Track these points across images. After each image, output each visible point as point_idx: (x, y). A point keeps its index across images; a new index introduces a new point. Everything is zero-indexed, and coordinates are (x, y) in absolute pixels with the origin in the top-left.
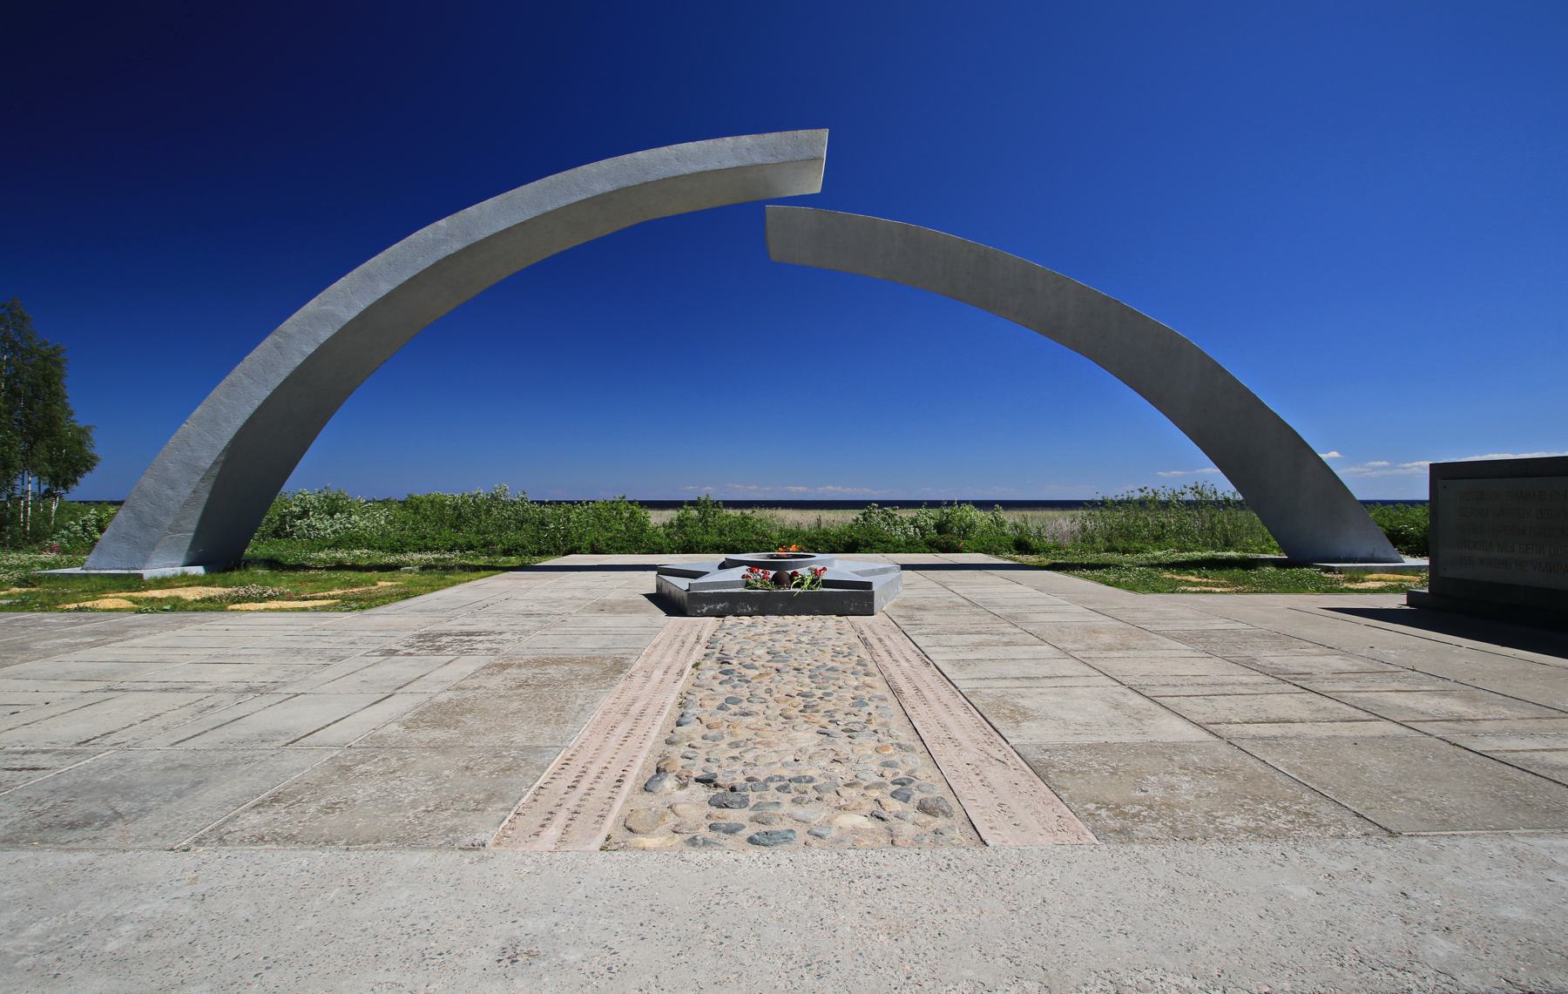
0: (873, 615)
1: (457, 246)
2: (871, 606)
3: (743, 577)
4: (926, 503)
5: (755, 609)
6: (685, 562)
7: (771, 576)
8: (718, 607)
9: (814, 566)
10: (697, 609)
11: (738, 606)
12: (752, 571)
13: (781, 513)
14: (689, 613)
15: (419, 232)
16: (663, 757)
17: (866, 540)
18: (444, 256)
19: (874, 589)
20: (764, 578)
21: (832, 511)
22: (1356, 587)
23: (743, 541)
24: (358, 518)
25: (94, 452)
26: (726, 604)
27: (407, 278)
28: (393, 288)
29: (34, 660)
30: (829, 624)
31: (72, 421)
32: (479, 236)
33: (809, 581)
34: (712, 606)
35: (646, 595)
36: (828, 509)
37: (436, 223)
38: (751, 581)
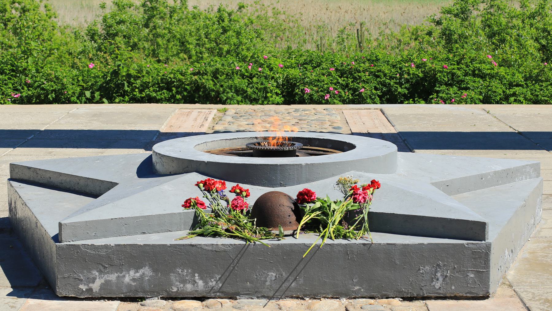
0: (485, 297)
3: (187, 204)
5: (212, 283)
6: (48, 158)
7: (251, 201)
8: (127, 279)
9: (351, 175)
11: (173, 277)
12: (208, 187)
14: (60, 292)
17: (453, 74)
20: (235, 207)
22: (313, 151)
23: (215, 74)
24: (143, 96)
29: (328, 298)
33: (338, 217)
34: (113, 277)
38: (205, 215)
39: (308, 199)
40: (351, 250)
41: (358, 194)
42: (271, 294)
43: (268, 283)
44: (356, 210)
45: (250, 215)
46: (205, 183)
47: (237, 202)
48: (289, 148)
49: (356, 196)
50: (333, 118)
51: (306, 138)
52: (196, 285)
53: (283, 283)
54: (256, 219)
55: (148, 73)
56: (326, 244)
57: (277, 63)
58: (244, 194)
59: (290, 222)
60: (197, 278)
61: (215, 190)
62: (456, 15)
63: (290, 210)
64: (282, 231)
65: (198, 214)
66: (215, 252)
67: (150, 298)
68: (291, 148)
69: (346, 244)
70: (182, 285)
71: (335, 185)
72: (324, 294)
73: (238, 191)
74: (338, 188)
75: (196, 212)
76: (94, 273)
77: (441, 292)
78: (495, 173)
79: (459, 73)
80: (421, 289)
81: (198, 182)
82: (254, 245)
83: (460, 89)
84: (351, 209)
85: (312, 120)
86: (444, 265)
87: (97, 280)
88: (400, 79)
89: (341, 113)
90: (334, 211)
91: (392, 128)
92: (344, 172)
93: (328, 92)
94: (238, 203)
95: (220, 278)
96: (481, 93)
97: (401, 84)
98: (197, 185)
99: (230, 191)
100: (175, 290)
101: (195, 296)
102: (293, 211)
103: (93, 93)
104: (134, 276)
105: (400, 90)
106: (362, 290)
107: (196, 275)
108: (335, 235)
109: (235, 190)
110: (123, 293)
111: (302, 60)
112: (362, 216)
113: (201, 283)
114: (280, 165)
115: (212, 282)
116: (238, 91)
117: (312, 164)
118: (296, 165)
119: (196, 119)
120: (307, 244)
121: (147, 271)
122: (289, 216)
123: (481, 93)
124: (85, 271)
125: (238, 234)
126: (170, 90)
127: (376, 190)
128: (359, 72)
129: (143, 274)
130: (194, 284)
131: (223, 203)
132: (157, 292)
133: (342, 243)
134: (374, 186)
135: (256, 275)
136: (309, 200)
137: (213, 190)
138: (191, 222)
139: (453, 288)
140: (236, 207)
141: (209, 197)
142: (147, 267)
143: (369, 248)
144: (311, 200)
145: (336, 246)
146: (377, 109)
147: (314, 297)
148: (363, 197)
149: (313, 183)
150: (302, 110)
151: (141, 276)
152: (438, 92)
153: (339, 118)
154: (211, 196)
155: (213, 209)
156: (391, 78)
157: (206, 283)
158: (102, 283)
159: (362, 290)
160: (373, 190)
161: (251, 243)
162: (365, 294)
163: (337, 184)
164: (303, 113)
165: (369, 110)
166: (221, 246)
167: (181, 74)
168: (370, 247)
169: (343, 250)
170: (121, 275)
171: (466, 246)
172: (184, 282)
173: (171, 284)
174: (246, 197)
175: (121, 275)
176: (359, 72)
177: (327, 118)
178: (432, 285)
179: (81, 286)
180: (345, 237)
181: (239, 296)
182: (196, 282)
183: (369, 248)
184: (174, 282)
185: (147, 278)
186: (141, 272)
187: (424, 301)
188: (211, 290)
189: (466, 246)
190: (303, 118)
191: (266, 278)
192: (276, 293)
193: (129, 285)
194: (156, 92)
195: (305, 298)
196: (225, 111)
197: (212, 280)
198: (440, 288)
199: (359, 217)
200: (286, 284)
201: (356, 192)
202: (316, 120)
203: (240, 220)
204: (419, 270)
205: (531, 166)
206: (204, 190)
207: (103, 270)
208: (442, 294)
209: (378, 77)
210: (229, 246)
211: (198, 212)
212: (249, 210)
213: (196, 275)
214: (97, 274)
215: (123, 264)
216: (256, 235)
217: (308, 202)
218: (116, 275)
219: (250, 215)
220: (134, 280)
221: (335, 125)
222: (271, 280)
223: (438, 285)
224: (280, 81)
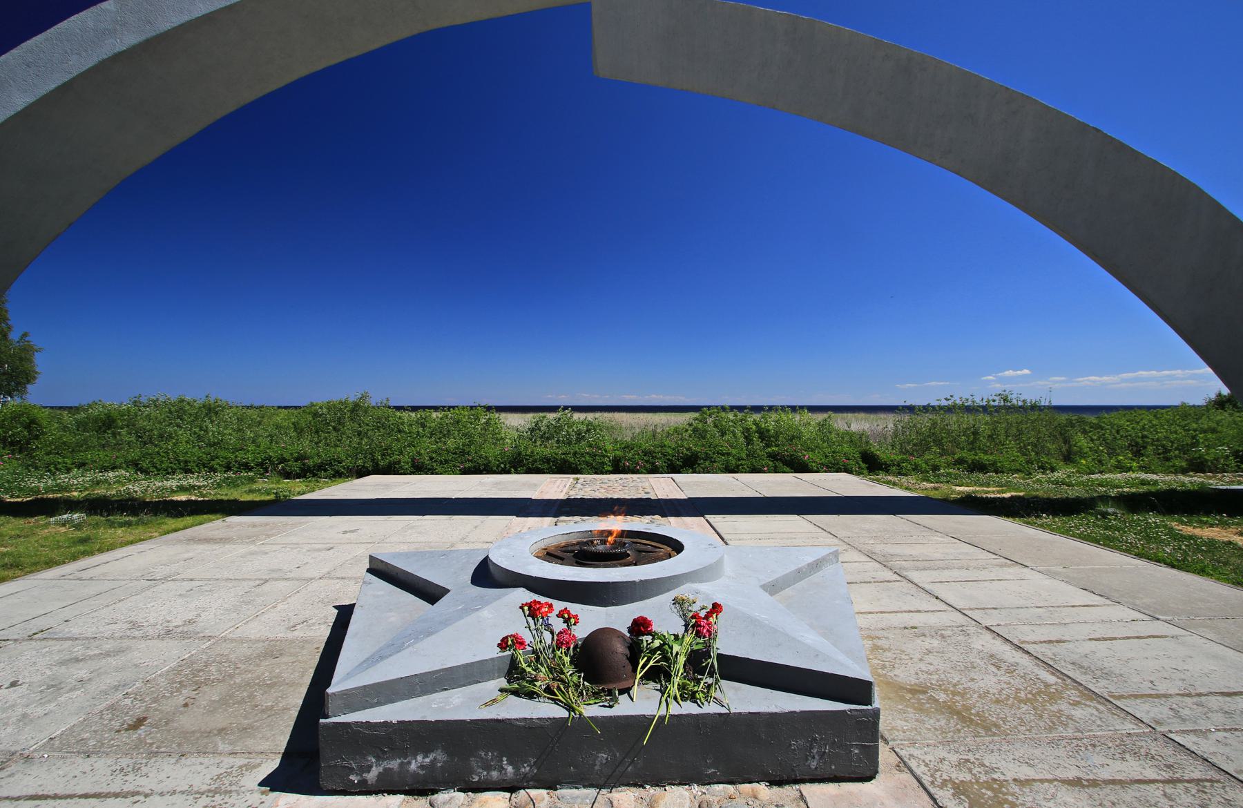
0: (869, 778)
1: (130, 39)
2: (774, 594)
3: (503, 645)
5: (525, 769)
8: (413, 766)
10: (351, 770)
11: (474, 763)
12: (533, 611)
13: (618, 416)
14: (324, 784)
15: (73, 18)
17: (707, 454)
18: (110, 54)
21: (668, 414)
25: (37, 370)
26: (438, 756)
27: (53, 86)
28: (31, 101)
31: (27, 341)
32: (164, 25)
34: (394, 764)
35: (355, 604)
37: (98, 6)
42: (601, 782)
43: (597, 768)
45: (578, 650)
46: (530, 605)
52: (503, 772)
53: (617, 767)
54: (582, 675)
55: (537, 453)
57: (609, 447)
58: (573, 621)
60: (505, 762)
62: (700, 421)
63: (625, 658)
64: (617, 695)
67: (444, 790)
70: (485, 773)
72: (669, 779)
73: (566, 616)
74: (676, 610)
75: (513, 654)
76: (369, 759)
77: (818, 773)
78: (808, 565)
79: (710, 453)
80: (793, 770)
82: (579, 718)
83: (711, 462)
84: (695, 647)
86: (821, 739)
87: (374, 768)
88: (678, 456)
92: (677, 586)
93: (639, 465)
95: (535, 763)
96: (723, 464)
97: (678, 460)
98: (521, 608)
100: (476, 779)
101: (502, 786)
102: (628, 659)
103: (505, 465)
104: (423, 762)
105: (678, 463)
106: (718, 773)
107: (505, 759)
109: (562, 615)
110: (407, 785)
111: (623, 446)
113: (510, 769)
114: (612, 583)
115: (525, 768)
116: (588, 464)
119: (558, 487)
121: (439, 756)
122: (624, 667)
123: (723, 464)
124: (358, 757)
125: (560, 698)
126: (548, 463)
128: (655, 453)
129: (435, 759)
130: (501, 772)
131: (547, 636)
132: (453, 783)
135: (582, 758)
139: (833, 767)
140: (562, 643)
141: (533, 627)
142: (440, 751)
147: (657, 783)
148: (708, 631)
151: (431, 761)
152: (699, 464)
153: (647, 484)
154: (535, 624)
156: (673, 456)
157: (516, 768)
158: (380, 773)
159: (718, 773)
162: (723, 779)
163: (673, 604)
166: (537, 721)
167: (555, 454)
170: (406, 761)
171: (849, 713)
172: (488, 768)
173: (472, 772)
175: (406, 761)
176: (655, 453)
178: (807, 764)
179: (352, 777)
180: (693, 697)
181: (560, 785)
182: (503, 768)
184: (475, 768)
185: (439, 765)
186: (431, 756)
187: (797, 787)
188: (523, 778)
189: (849, 713)
191: (595, 760)
192: (608, 779)
193: (415, 774)
194: (541, 464)
195: (646, 786)
196: (578, 479)
197: (526, 765)
198: (816, 768)
200: (621, 769)
204: (790, 745)
205: (832, 553)
207: (382, 756)
208: (820, 775)
209: (665, 455)
213: (505, 759)
214: (374, 760)
215: (407, 747)
218: (399, 761)
219: (578, 650)
220: (422, 767)
222: (601, 764)
223: (814, 764)
224: (611, 458)
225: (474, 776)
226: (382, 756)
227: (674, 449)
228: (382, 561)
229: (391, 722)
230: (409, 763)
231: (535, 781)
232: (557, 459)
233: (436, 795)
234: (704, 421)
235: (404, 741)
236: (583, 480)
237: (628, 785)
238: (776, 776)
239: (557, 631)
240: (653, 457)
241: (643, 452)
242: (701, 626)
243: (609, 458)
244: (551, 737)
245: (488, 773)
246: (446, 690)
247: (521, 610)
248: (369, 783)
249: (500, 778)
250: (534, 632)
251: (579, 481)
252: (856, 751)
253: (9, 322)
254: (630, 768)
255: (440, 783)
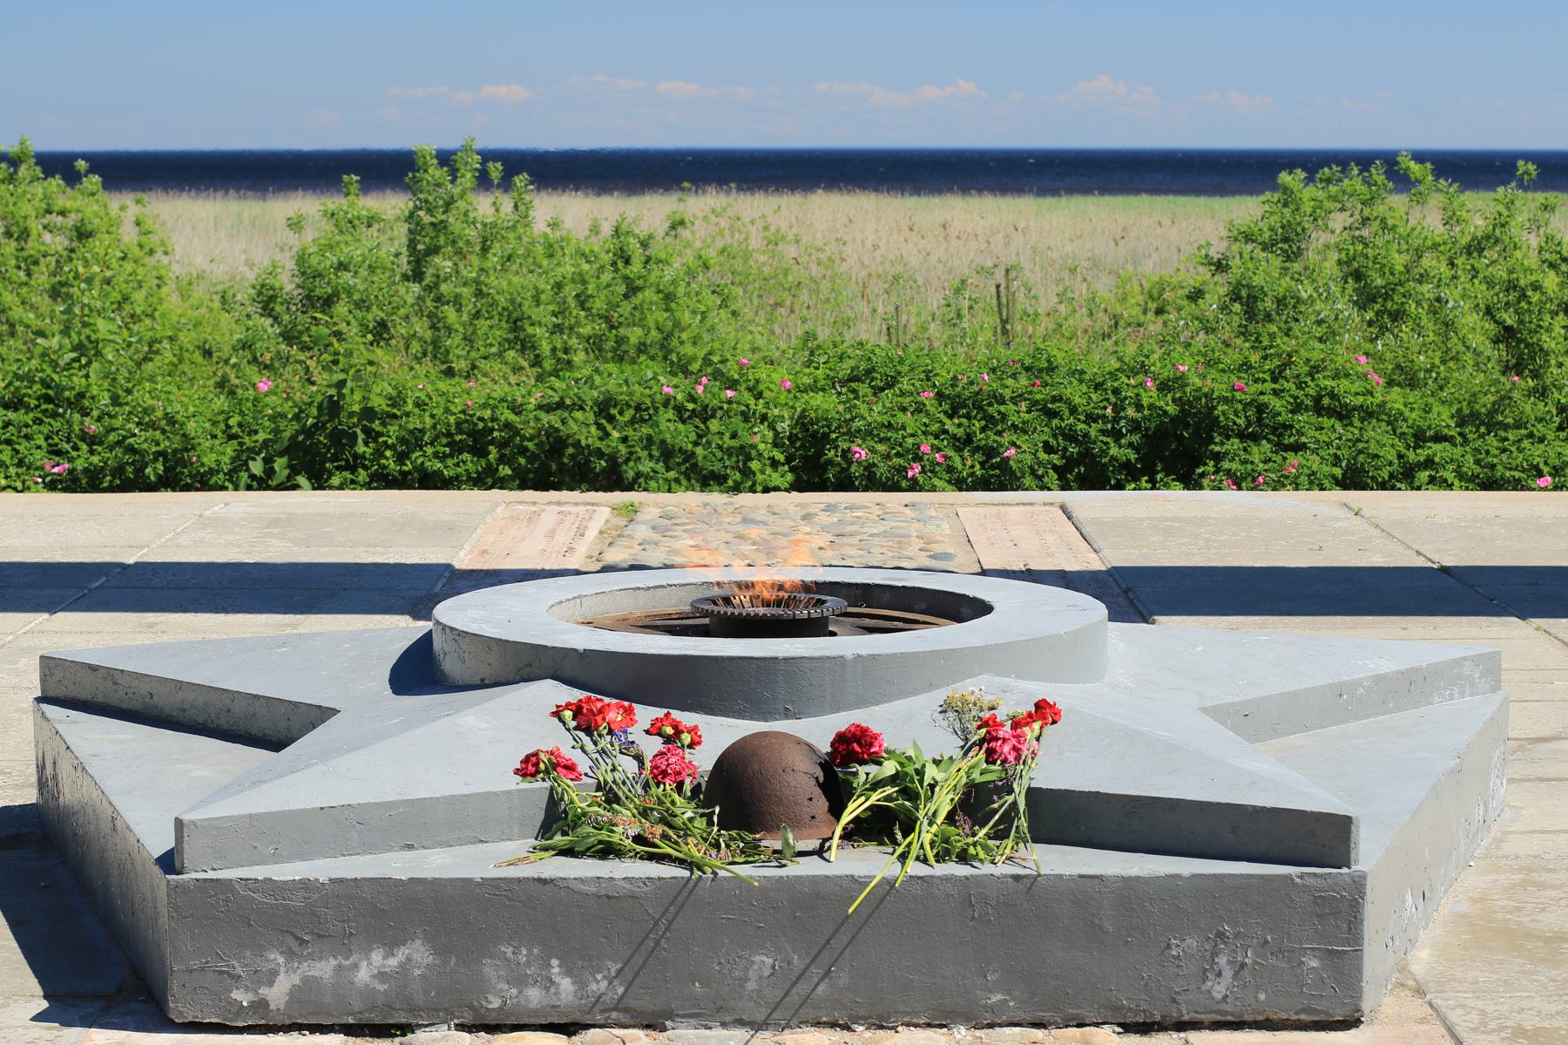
0: (1350, 1023)
3: (530, 767)
4: (1527, 168)
5: (599, 985)
7: (704, 760)
8: (363, 975)
9: (979, 688)
11: (489, 968)
14: (179, 1008)
16: (430, 348)
17: (1261, 408)
19: (1368, 853)
20: (660, 775)
30: (1084, 873)
33: (944, 802)
34: (324, 969)
36: (1042, 192)
38: (579, 796)
39: (863, 753)
40: (979, 894)
41: (1000, 739)
42: (760, 1016)
44: (994, 781)
45: (702, 796)
46: (578, 710)
47: (667, 760)
48: (809, 613)
49: (993, 744)
50: (930, 528)
51: (857, 585)
52: (552, 990)
53: (794, 984)
54: (717, 809)
55: (419, 404)
56: (911, 877)
59: (813, 817)
60: (556, 970)
61: (605, 728)
63: (813, 782)
64: (791, 841)
65: (557, 793)
66: (605, 900)
67: (427, 1026)
68: (815, 613)
69: (966, 878)
70: (514, 991)
71: (936, 715)
72: (907, 1013)
73: (669, 730)
75: (552, 788)
76: (272, 957)
77: (1227, 1008)
78: (1378, 679)
79: (1276, 404)
80: (1174, 1001)
81: (558, 707)
82: (713, 880)
83: (1282, 447)
85: (871, 535)
86: (1237, 935)
87: (282, 977)
89: (953, 515)
90: (932, 787)
91: (1094, 555)
94: (668, 765)
95: (619, 972)
97: (1117, 435)
98: (557, 714)
99: (647, 732)
100: (495, 1003)
102: (819, 785)
106: (1012, 1004)
107: (555, 962)
108: (935, 851)
109: (660, 728)
110: (353, 1014)
111: (845, 369)
112: (1010, 799)
113: (566, 985)
114: (785, 659)
115: (598, 982)
116: (667, 454)
117: (873, 657)
118: (829, 658)
119: (552, 534)
120: (859, 877)
121: (417, 953)
122: (811, 799)
126: (479, 452)
127: (1049, 729)
128: (1002, 402)
129: (409, 959)
130: (547, 989)
131: (629, 766)
133: (957, 874)
134: (1044, 718)
135: (720, 963)
136: (866, 756)
137: (601, 728)
138: (540, 817)
139: (1262, 997)
140: (664, 774)
143: (1030, 889)
144: (870, 754)
145: (939, 882)
146: (1052, 504)
148: (1014, 748)
149: (877, 708)
150: (846, 508)
151: (402, 965)
152: (1218, 457)
153: (946, 528)
155: (599, 782)
156: (1091, 418)
157: (581, 983)
158: (294, 986)
159: (1012, 1004)
160: (1041, 727)
161: (705, 873)
162: (1020, 1016)
163: (941, 712)
164: (849, 515)
165: (1029, 508)
168: (1032, 884)
169: (959, 894)
170: (348, 963)
171: (1299, 881)
172: (520, 981)
174: (691, 746)
175: (348, 963)
176: (1002, 402)
177: (914, 529)
178: (1204, 988)
180: (963, 857)
181: (673, 1020)
182: (552, 982)
183: (1030, 889)
184: (494, 981)
186: (402, 953)
187: (1182, 1035)
189: (1299, 881)
190: (849, 529)
191: (746, 970)
193: (369, 992)
194: (442, 458)
196: (632, 511)
197: (599, 977)
199: (1001, 802)
200: (802, 988)
201: (994, 734)
202: (885, 534)
203: (675, 810)
204: (1169, 947)
206: (576, 728)
207: (296, 949)
208: (1231, 1014)
210: (645, 884)
211: (560, 790)
212: (699, 785)
213: (555, 962)
214: (281, 960)
216: (719, 851)
217: (863, 762)
218: (333, 962)
219: (702, 796)
220: (382, 976)
221: (937, 548)
222: (760, 978)
223: (1219, 989)
225: (490, 997)
226: (296, 949)
227: (1098, 387)
228: (94, 669)
229: (318, 880)
230: (356, 966)
231: (626, 1011)
232: (517, 432)
233: (410, 1036)
234: (1287, 243)
235: (343, 921)
236: (657, 512)
237: (818, 1024)
238: (1136, 1013)
239: (648, 756)
240: (990, 421)
241: (940, 396)
242: (997, 739)
243: (772, 427)
244: (653, 918)
245: (520, 993)
246: (410, 847)
247: (556, 720)
248: (273, 1007)
249: (545, 1002)
250: (595, 756)
251: (639, 517)
252: (1314, 963)
253: (1490, 326)
254: (821, 988)
255: (421, 1010)
